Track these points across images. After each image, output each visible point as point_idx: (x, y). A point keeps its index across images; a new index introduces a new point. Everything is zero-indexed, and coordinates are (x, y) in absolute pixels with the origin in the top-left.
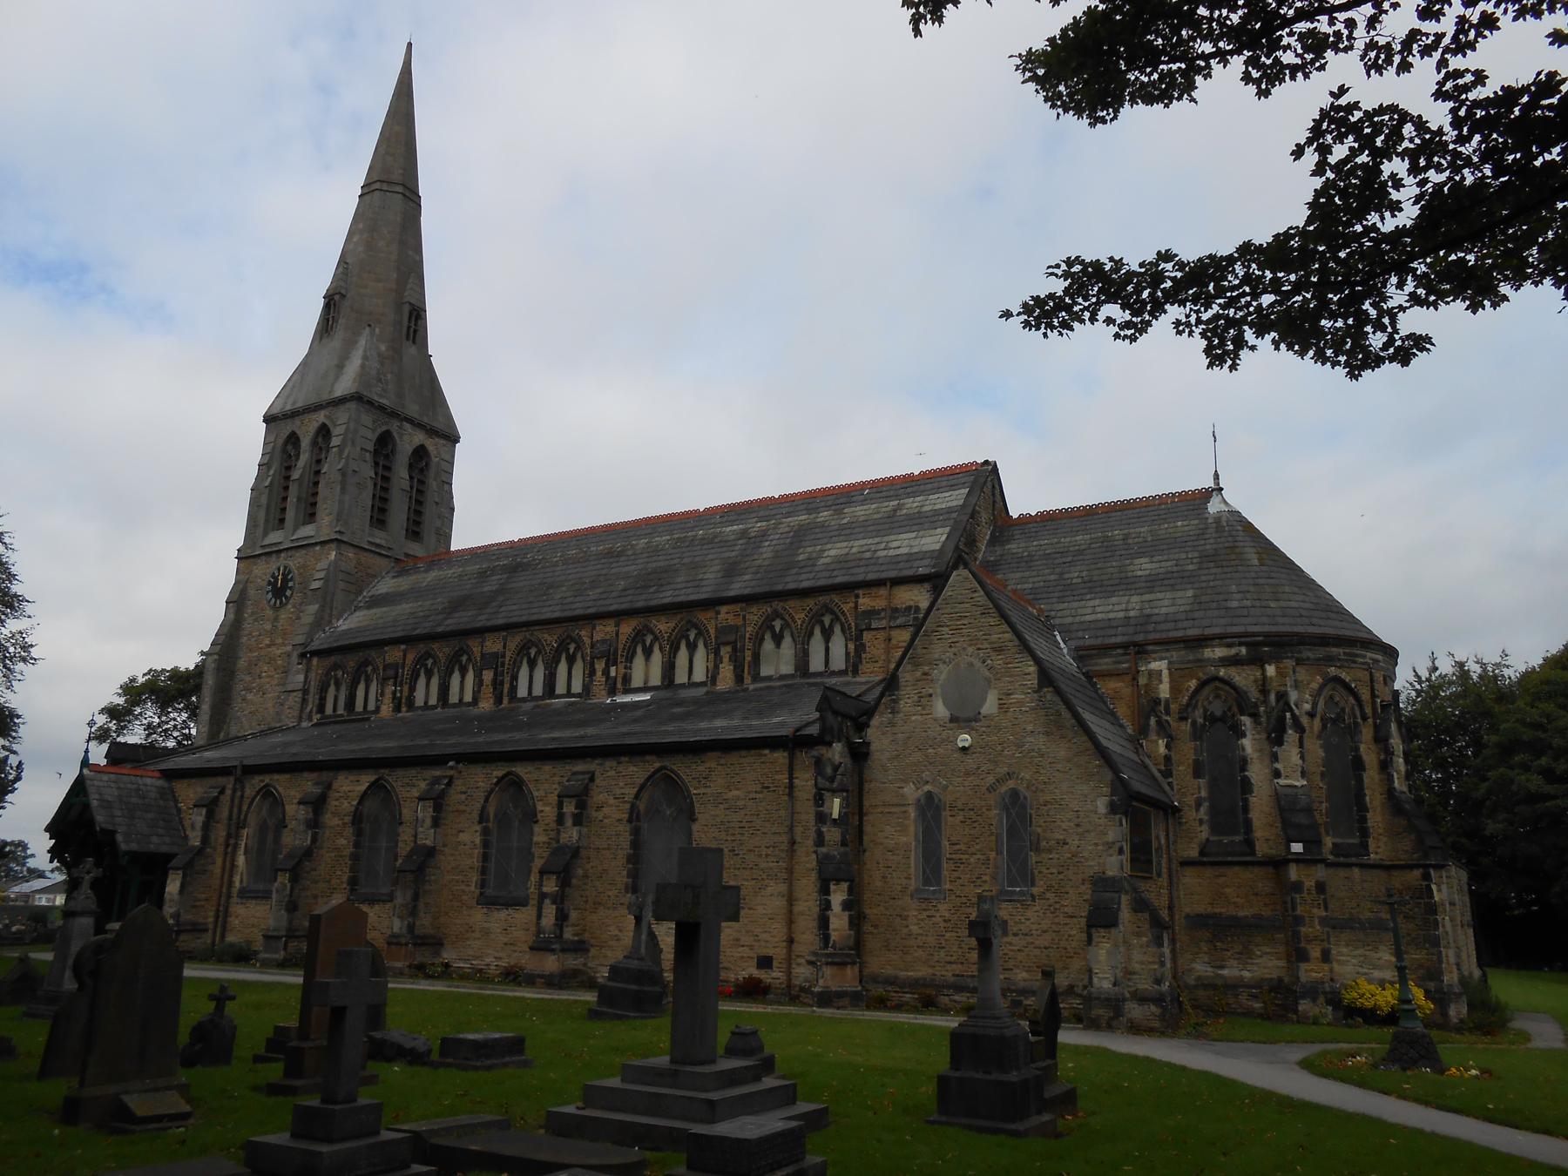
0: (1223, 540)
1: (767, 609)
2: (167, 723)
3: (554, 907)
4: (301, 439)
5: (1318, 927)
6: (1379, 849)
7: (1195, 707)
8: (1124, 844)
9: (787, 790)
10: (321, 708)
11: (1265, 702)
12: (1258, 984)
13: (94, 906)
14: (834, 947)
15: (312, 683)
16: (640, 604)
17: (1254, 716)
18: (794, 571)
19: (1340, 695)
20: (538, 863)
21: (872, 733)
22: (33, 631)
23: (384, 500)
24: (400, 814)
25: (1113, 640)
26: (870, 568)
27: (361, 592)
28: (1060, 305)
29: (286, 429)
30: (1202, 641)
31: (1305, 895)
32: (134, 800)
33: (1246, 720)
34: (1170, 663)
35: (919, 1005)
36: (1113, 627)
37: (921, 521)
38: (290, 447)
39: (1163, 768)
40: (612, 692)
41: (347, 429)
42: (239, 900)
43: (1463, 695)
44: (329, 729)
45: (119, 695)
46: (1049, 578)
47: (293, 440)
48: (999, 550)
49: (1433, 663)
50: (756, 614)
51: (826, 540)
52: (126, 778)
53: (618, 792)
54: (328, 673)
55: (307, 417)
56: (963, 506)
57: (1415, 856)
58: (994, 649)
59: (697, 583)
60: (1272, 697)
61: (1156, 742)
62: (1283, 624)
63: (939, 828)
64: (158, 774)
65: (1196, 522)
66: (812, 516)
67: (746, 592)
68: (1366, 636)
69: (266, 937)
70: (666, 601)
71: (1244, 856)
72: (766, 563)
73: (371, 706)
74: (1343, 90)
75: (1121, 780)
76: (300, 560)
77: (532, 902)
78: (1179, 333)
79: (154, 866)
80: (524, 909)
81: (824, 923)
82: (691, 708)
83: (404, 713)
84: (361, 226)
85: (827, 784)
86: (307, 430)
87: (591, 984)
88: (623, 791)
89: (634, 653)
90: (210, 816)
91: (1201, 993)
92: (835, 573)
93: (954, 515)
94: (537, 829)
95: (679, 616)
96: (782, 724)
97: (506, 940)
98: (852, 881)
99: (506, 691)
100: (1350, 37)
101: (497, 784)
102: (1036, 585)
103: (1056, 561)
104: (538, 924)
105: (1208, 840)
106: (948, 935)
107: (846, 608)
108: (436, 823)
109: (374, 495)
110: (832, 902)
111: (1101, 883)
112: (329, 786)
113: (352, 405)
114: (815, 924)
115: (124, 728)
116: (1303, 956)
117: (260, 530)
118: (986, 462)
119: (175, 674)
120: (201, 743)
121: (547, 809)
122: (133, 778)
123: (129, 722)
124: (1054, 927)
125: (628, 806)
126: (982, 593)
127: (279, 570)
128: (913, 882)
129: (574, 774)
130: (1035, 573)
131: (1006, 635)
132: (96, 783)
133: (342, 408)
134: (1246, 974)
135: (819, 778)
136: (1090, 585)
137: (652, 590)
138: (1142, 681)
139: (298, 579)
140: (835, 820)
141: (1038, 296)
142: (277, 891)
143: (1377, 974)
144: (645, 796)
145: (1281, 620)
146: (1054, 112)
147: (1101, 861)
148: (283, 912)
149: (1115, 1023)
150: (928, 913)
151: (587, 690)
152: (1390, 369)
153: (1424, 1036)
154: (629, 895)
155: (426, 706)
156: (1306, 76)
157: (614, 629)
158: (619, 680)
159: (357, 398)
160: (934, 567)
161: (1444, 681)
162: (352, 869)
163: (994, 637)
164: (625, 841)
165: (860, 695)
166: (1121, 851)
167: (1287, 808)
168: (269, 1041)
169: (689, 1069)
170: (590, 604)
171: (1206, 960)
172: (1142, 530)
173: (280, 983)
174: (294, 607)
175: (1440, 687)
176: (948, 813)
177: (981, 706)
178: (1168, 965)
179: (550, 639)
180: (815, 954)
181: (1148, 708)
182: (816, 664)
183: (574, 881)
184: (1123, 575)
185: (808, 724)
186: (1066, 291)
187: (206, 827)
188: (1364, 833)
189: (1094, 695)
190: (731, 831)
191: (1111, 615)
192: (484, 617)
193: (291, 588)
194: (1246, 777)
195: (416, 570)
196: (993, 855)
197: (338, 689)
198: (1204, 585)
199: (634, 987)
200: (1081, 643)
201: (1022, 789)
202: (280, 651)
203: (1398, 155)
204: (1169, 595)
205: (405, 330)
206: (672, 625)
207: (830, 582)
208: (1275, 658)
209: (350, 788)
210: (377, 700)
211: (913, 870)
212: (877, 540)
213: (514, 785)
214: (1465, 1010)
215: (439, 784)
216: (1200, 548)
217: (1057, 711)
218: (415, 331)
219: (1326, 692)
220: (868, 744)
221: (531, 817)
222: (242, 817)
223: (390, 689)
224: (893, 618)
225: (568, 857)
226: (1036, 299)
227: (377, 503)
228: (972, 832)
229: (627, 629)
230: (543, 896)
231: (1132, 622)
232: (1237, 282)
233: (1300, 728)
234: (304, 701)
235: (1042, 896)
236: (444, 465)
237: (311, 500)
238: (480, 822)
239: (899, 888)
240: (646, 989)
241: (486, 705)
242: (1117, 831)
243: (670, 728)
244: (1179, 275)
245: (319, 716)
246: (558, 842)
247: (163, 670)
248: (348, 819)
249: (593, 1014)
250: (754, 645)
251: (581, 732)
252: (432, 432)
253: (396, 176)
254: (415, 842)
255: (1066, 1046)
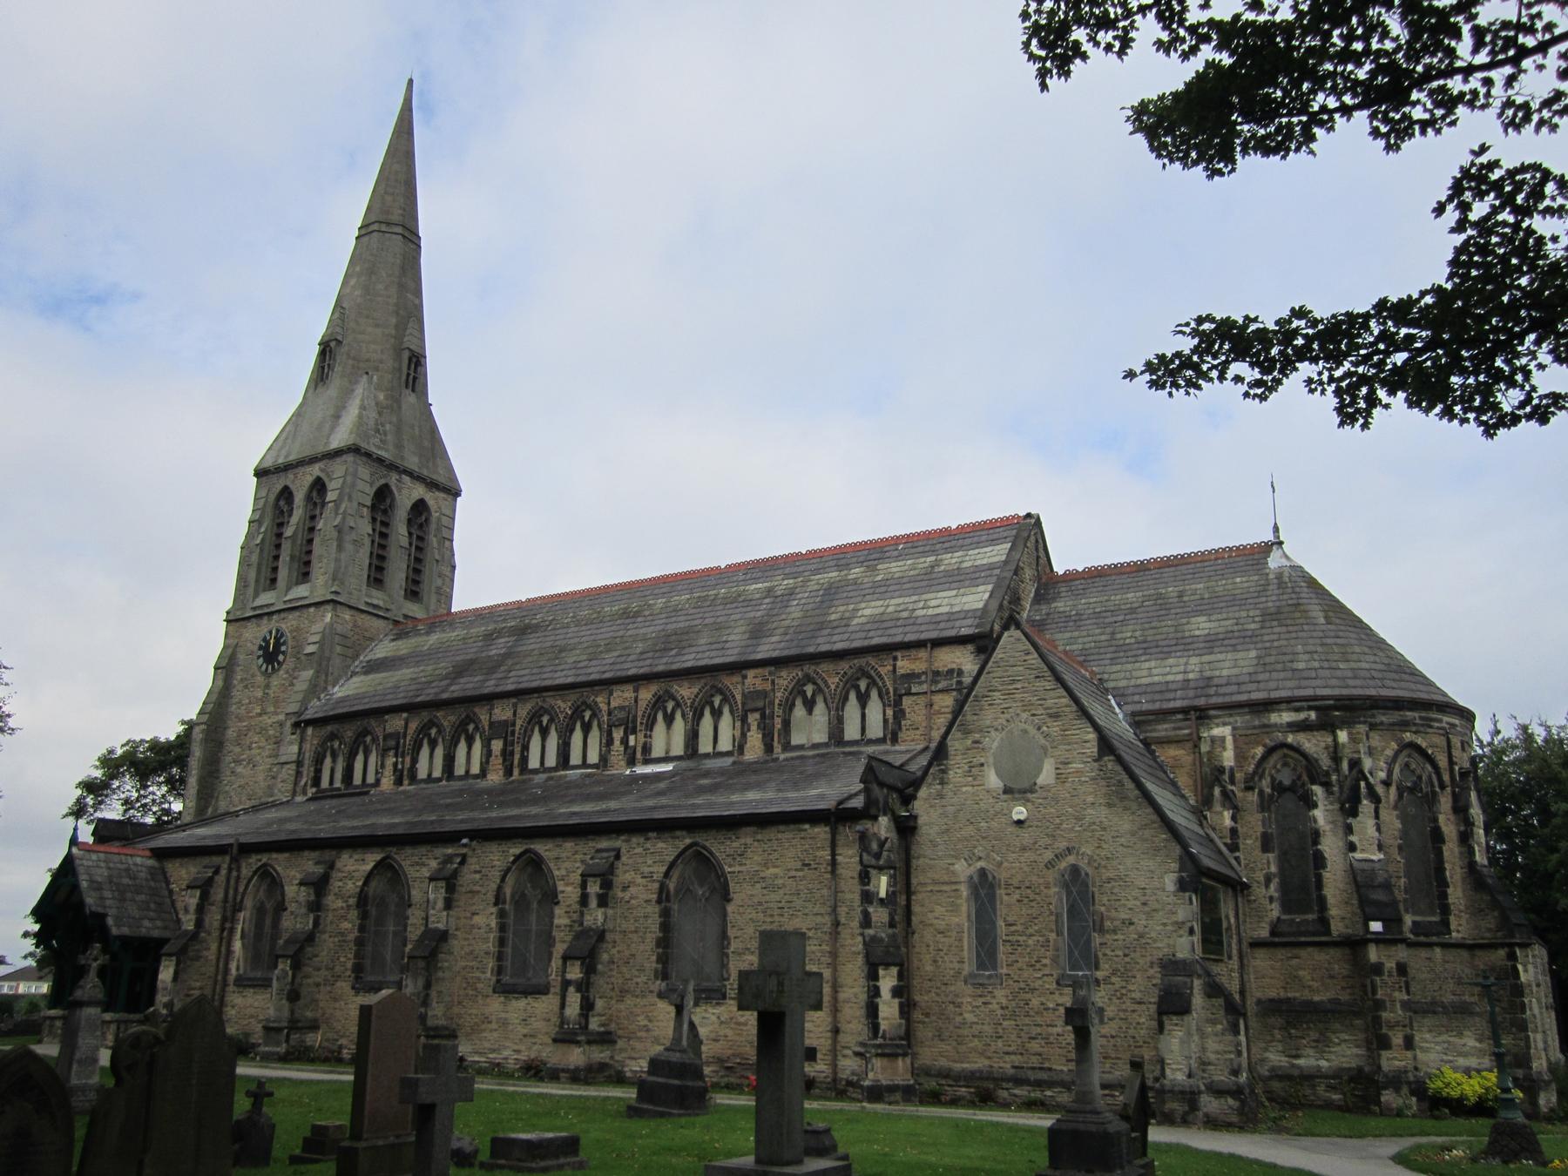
0: (1285, 597)
1: (798, 673)
2: (145, 797)
3: (579, 995)
4: (295, 493)
5: (1400, 1012)
6: (1460, 928)
7: (1262, 777)
8: (1195, 924)
9: (829, 868)
10: (316, 781)
11: (1338, 770)
12: (1337, 1074)
13: (101, 996)
14: (884, 1037)
15: (307, 755)
16: (660, 668)
17: (1327, 785)
18: (826, 632)
19: (1416, 763)
20: (559, 949)
21: (919, 806)
22: (11, 700)
23: (382, 558)
24: (409, 896)
25: (1172, 705)
26: (908, 629)
27: (358, 656)
28: (1186, 363)
29: (278, 484)
30: (1268, 705)
31: (1385, 977)
32: (126, 881)
33: (1318, 790)
34: (1234, 729)
35: (976, 1099)
36: (1171, 691)
37: (961, 578)
38: (282, 503)
39: (1229, 841)
40: (631, 762)
41: (344, 483)
42: (235, 989)
43: (1528, 759)
44: (327, 804)
45: (97, 767)
46: (1098, 638)
47: (286, 495)
48: (1044, 608)
49: (1495, 725)
50: (785, 678)
51: (859, 599)
52: (116, 858)
53: (646, 870)
54: (323, 744)
55: (301, 470)
56: (1006, 562)
57: (1499, 934)
58: (1050, 716)
59: (719, 646)
60: (1345, 765)
61: (1221, 813)
62: (1354, 687)
63: (994, 910)
64: (148, 853)
65: (1256, 578)
66: (843, 573)
67: (775, 654)
68: (1445, 699)
69: (267, 1029)
70: (689, 664)
71: (1318, 934)
72: (795, 623)
73: (371, 779)
74: (1483, 149)
75: (1191, 855)
76: (294, 623)
77: (552, 990)
78: (1312, 391)
79: (146, 952)
80: (544, 997)
81: (872, 1011)
82: (718, 780)
83: (406, 787)
84: (358, 269)
85: (873, 862)
86: (300, 484)
87: (619, 1079)
88: (651, 869)
89: (654, 720)
90: (205, 897)
91: (1276, 1085)
92: (871, 634)
93: (997, 572)
94: (558, 911)
95: (703, 681)
96: (822, 797)
97: (525, 1031)
98: (901, 965)
99: (516, 762)
100: (1488, 95)
101: (514, 862)
102: (1087, 646)
103: (1107, 620)
104: (562, 1014)
105: (1279, 918)
106: (1005, 1023)
107: (883, 671)
108: (448, 905)
109: (371, 553)
110: (882, 988)
111: (1171, 966)
112: (332, 866)
113: (350, 458)
114: (863, 1012)
115: (101, 803)
116: (1385, 1043)
117: (251, 590)
118: (1029, 515)
119: (155, 745)
120: (187, 819)
121: (569, 889)
122: (123, 857)
123: (107, 796)
124: (1122, 1015)
125: (656, 885)
126: (1036, 655)
127: (271, 633)
128: (966, 966)
129: (598, 851)
130: (1085, 633)
131: (1063, 700)
132: (85, 863)
133: (338, 460)
134: (1323, 1063)
135: (864, 854)
136: (1145, 645)
137: (674, 652)
138: (1204, 748)
139: (290, 643)
140: (882, 900)
141: (1164, 355)
142: (278, 979)
143: (1462, 1062)
144: (675, 874)
145: (1351, 682)
146: (1160, 163)
147: (1171, 942)
148: (284, 1001)
149: (1190, 1118)
150: (983, 1000)
151: (604, 760)
152: (1527, 428)
153: (1525, 1126)
154: (658, 982)
155: (543, 768)
156: (1438, 132)
157: (633, 695)
158: (639, 750)
159: (355, 450)
160: (977, 627)
161: (1508, 746)
162: (357, 956)
163: (1050, 703)
164: (654, 923)
165: (902, 765)
166: (1191, 931)
167: (1362, 882)
168: (306, 1140)
169: (776, 1169)
170: (607, 668)
171: (1280, 1048)
172: (1199, 586)
173: (285, 1079)
174: (287, 672)
175: (1503, 752)
176: (1003, 892)
177: (1037, 776)
178: (1245, 1055)
179: (564, 706)
180: (862, 1044)
181: (1212, 778)
182: (852, 732)
183: (600, 967)
184: (1180, 635)
185: (851, 797)
186: (1195, 350)
187: (201, 909)
188: (1445, 910)
189: (1151, 763)
190: (769, 912)
191: (1170, 678)
192: (492, 682)
193: (283, 653)
194: (1318, 850)
195: (417, 633)
196: (1053, 936)
197: (334, 761)
198: (1268, 645)
199: (676, 1082)
200: (1137, 708)
201: (1083, 864)
202: (270, 721)
203: (1540, 212)
204: (1230, 656)
205: (404, 377)
206: (695, 690)
207: (866, 643)
208: (1347, 724)
209: (355, 868)
210: (377, 772)
211: (965, 953)
212: (914, 598)
213: (533, 865)
214: (1554, 1099)
215: (452, 863)
216: (1261, 606)
217: (1119, 781)
218: (415, 379)
219: (1402, 759)
220: (915, 818)
221: (551, 897)
222: (239, 898)
223: (390, 761)
224: (935, 682)
225: (593, 941)
226: (1161, 358)
227: (375, 562)
228: (1029, 912)
229: (647, 694)
230: (566, 984)
231: (1192, 684)
232: (1372, 339)
233: (1375, 799)
234: (298, 774)
235: (1107, 980)
236: (445, 520)
237: (306, 559)
238: (496, 904)
239: (952, 972)
240: (690, 1083)
241: (495, 777)
242: (1187, 909)
243: (699, 801)
244: (1310, 331)
245: (314, 790)
246: (581, 924)
247: (142, 741)
248: (352, 901)
249: (633, 1112)
250: (784, 711)
251: (603, 806)
252: (433, 485)
253: (395, 216)
254: (427, 925)
255: (1158, 1145)
